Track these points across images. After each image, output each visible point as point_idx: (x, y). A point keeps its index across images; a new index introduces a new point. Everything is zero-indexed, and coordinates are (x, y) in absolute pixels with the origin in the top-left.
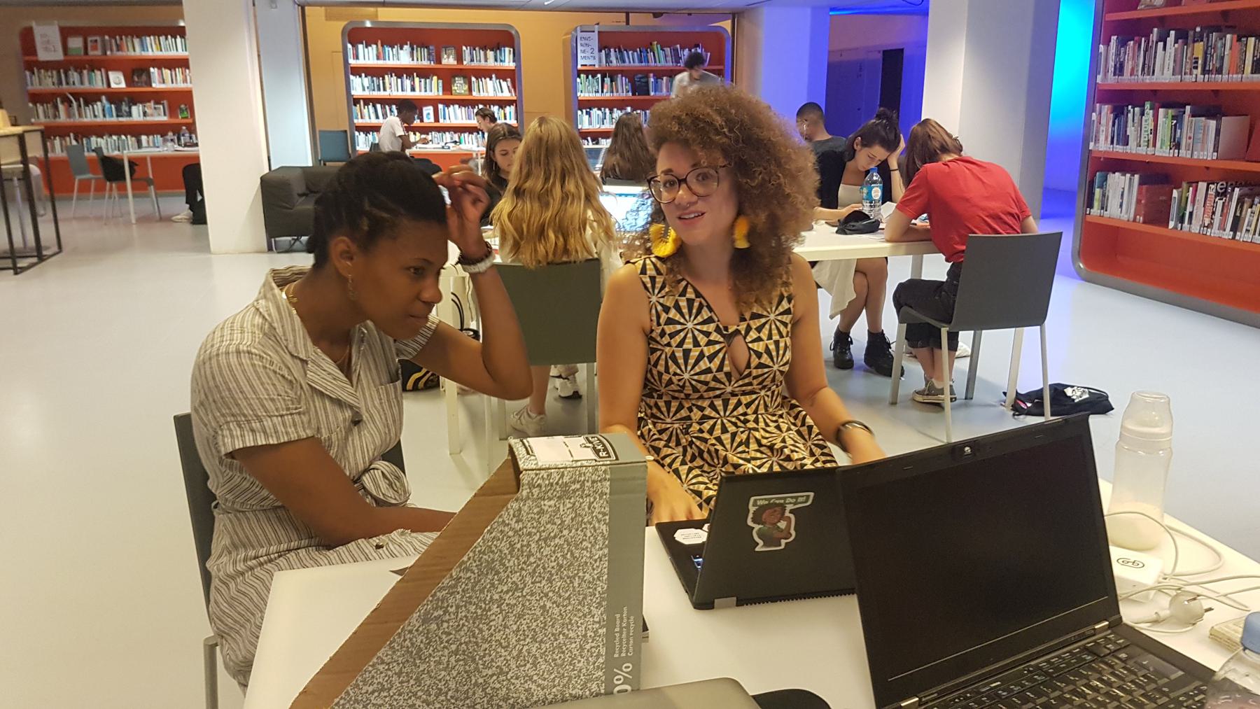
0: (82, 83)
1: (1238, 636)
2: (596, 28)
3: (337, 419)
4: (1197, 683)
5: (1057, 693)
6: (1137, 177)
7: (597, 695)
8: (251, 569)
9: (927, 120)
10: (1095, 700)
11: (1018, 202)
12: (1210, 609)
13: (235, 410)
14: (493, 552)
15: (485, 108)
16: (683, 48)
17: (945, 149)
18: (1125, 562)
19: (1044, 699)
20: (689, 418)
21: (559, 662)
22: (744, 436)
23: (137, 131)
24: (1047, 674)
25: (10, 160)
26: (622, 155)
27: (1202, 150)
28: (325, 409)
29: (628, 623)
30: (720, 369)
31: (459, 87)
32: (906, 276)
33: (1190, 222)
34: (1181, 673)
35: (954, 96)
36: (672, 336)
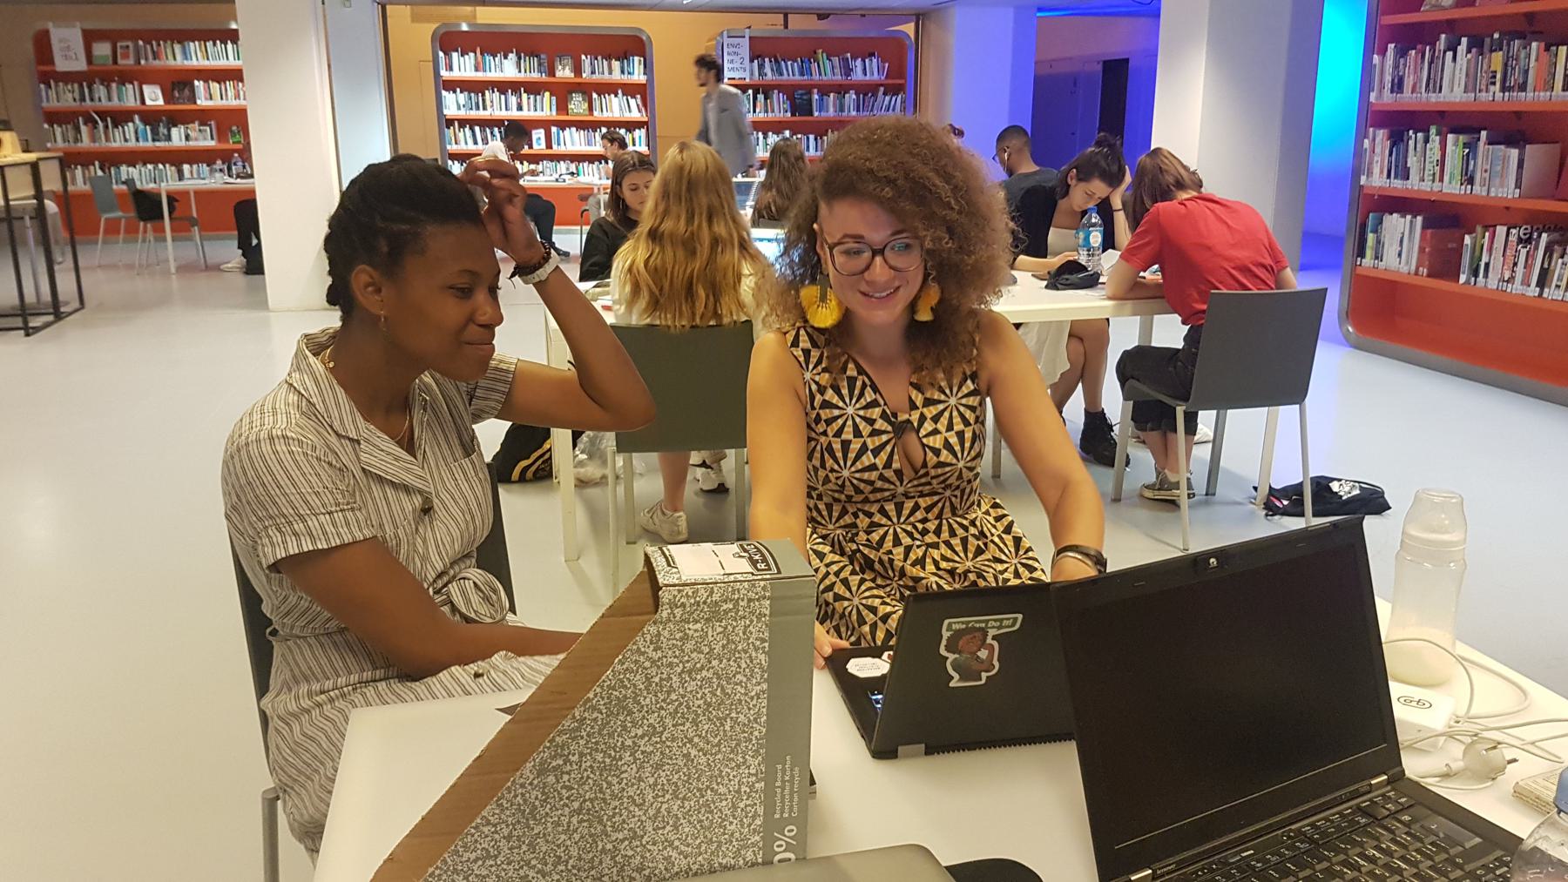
0: (110, 99)
4: (1499, 853)
5: (1325, 864)
6: (1419, 218)
7: (753, 865)
8: (319, 705)
9: (1158, 150)
10: (1371, 873)
11: (1272, 250)
12: (1515, 760)
13: (273, 511)
15: (614, 132)
16: (854, 58)
17: (1180, 185)
18: (1407, 701)
19: (1308, 872)
21: (706, 823)
22: (920, 552)
23: (178, 158)
24: (1311, 840)
25: (20, 192)
26: (779, 191)
27: (1502, 186)
29: (792, 776)
30: (888, 465)
31: (577, 106)
32: (1132, 343)
34: (1478, 840)
35: (1191, 120)
36: (829, 422)
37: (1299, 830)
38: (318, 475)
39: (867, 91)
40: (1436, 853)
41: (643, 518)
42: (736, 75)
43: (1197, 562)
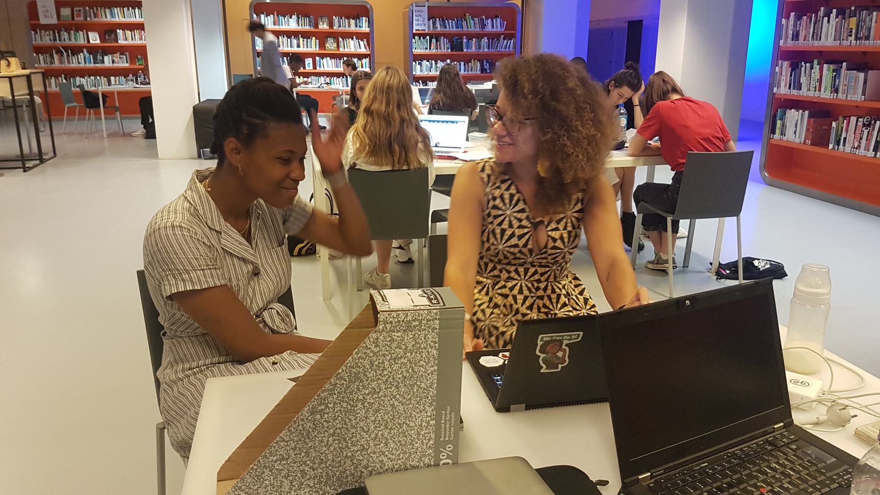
0: (70, 40)
1: (875, 436)
2: (427, 4)
3: (242, 271)
4: (846, 467)
5: (748, 472)
6: (807, 112)
7: (429, 466)
8: (188, 376)
9: (660, 73)
11: (723, 130)
13: (172, 266)
14: (359, 367)
15: (349, 60)
16: (487, 18)
18: (796, 382)
19: (738, 476)
20: (499, 276)
21: (403, 443)
23: (108, 73)
24: (740, 458)
26: (445, 94)
28: (234, 265)
29: (451, 418)
30: (525, 245)
31: (331, 45)
33: (844, 145)
35: (679, 55)
36: (496, 217)
37: (734, 452)
38: (197, 249)
39: (494, 37)
40: (811, 467)
41: (366, 277)
42: (420, 28)
43: (680, 302)
